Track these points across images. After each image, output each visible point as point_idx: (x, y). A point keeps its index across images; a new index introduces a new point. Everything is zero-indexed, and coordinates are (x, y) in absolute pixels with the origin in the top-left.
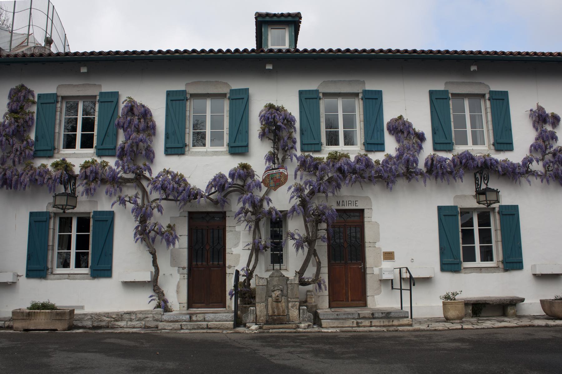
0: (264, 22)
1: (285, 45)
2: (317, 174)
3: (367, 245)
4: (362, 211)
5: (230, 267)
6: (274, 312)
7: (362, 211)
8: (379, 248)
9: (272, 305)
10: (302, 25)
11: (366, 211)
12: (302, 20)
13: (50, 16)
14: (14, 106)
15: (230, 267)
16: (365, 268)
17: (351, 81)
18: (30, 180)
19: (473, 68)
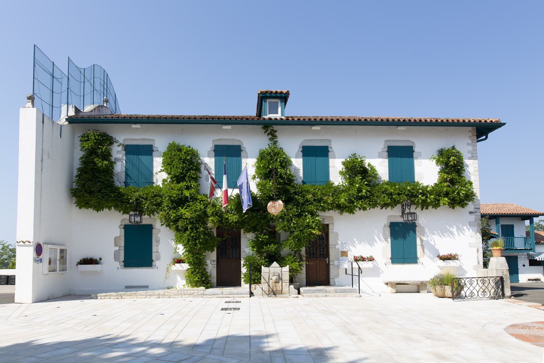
0: (263, 97)
1: (277, 113)
3: (330, 246)
4: (328, 225)
7: (328, 225)
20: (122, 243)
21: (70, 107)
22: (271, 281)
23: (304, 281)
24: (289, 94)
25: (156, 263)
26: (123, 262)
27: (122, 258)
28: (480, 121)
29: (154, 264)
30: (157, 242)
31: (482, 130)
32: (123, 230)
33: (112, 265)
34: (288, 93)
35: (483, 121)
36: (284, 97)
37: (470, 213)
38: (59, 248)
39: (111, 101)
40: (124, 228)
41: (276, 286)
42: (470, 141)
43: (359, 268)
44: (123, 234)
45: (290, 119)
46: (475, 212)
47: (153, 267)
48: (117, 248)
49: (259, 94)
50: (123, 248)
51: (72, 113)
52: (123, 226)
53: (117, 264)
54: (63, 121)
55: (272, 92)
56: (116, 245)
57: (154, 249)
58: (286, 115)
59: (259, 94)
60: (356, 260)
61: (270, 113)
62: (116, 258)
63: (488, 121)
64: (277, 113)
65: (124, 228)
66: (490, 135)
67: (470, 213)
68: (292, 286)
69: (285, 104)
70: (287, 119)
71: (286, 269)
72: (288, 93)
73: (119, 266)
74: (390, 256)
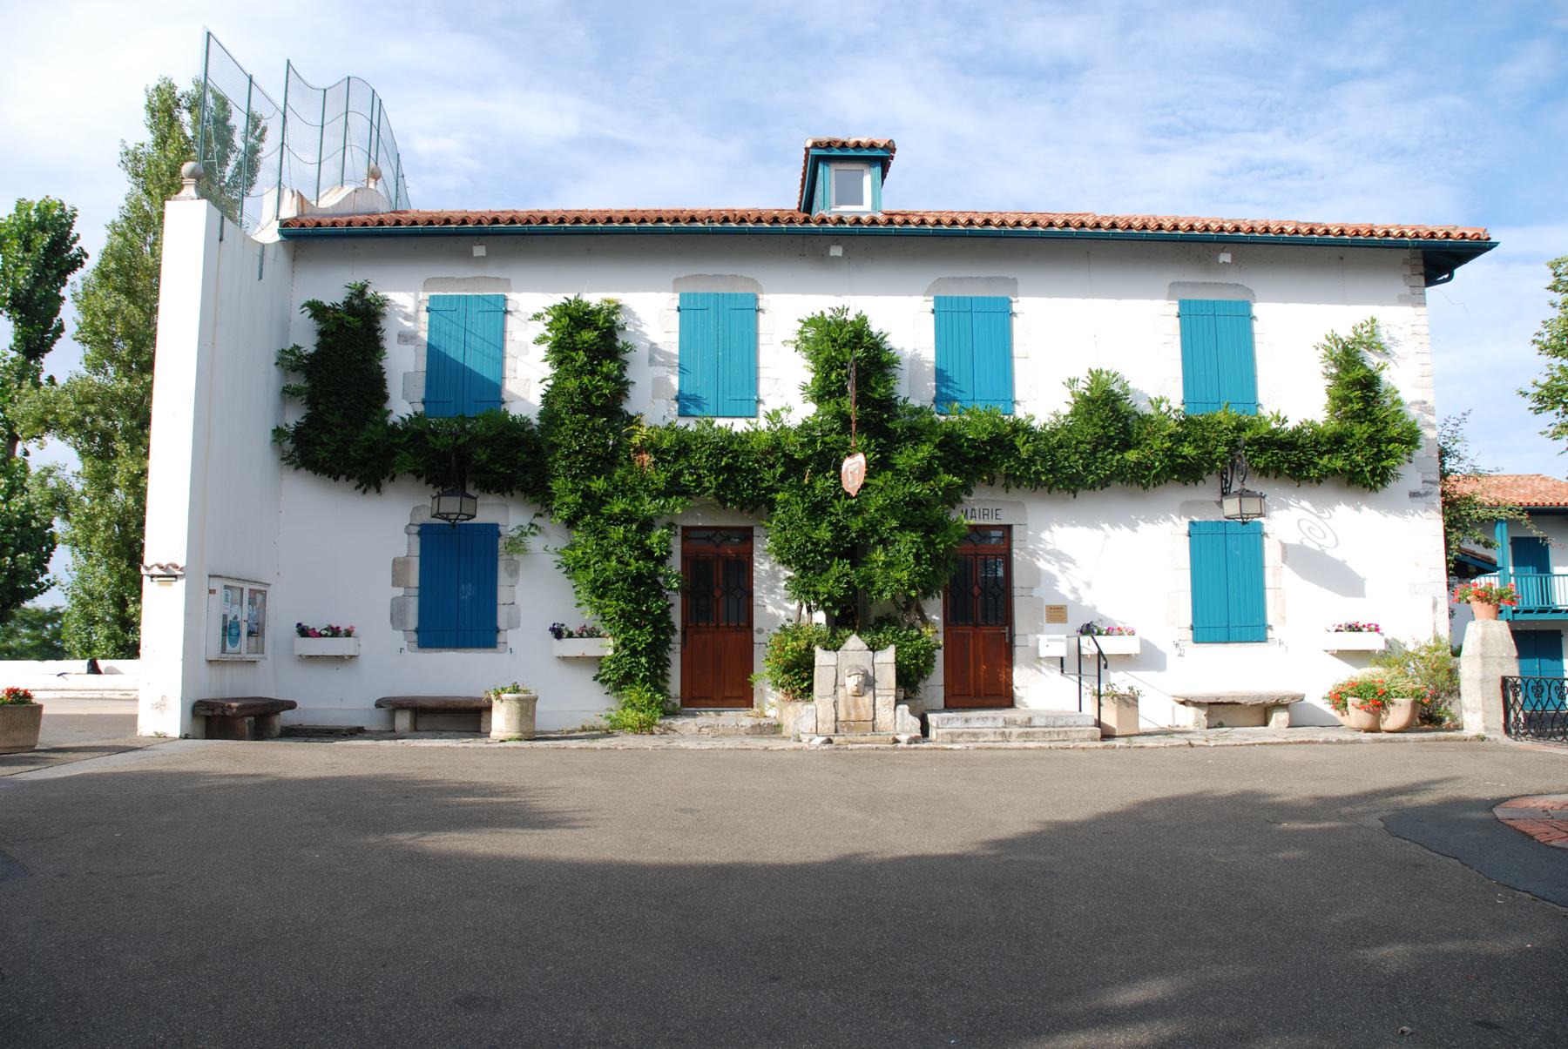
0: (823, 156)
1: (861, 203)
2: (69, 397)
3: (1016, 592)
4: (1009, 528)
5: (761, 631)
6: (849, 714)
7: (1009, 528)
8: (1040, 599)
9: (846, 701)
10: (893, 163)
11: (1015, 530)
12: (896, 155)
13: (373, 155)
14: (148, 378)
15: (761, 631)
16: (1012, 636)
17: (960, 279)
18: (1528, 718)
19: (1225, 258)
20: (414, 579)
21: (287, 195)
22: (841, 691)
23: (940, 700)
24: (894, 150)
25: (508, 636)
26: (417, 631)
27: (413, 622)
28: (1432, 235)
29: (501, 638)
30: (511, 576)
31: (1437, 259)
32: (416, 541)
33: (709, 497)
34: (890, 148)
35: (1440, 234)
36: (879, 158)
37: (1413, 495)
38: (247, 587)
39: (387, 171)
40: (420, 533)
41: (856, 706)
42: (1407, 290)
43: (1100, 653)
44: (416, 551)
45: (898, 219)
46: (1426, 494)
47: (500, 647)
48: (400, 592)
49: (807, 149)
50: (415, 592)
51: (289, 211)
52: (416, 529)
53: (399, 638)
54: (269, 234)
55: (844, 145)
56: (395, 584)
57: (503, 595)
58: (887, 208)
59: (807, 149)
60: (1088, 630)
61: (839, 203)
62: (397, 618)
63: (1455, 234)
64: (861, 203)
65: (420, 533)
66: (1457, 271)
67: (1413, 495)
68: (904, 708)
69: (884, 177)
70: (890, 222)
71: (888, 656)
72: (890, 148)
73: (404, 644)
74: (1189, 621)
